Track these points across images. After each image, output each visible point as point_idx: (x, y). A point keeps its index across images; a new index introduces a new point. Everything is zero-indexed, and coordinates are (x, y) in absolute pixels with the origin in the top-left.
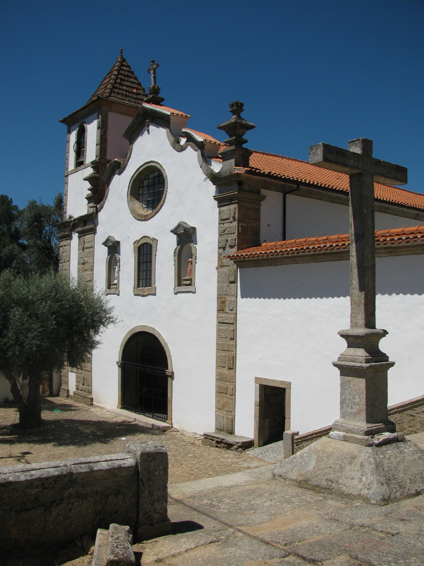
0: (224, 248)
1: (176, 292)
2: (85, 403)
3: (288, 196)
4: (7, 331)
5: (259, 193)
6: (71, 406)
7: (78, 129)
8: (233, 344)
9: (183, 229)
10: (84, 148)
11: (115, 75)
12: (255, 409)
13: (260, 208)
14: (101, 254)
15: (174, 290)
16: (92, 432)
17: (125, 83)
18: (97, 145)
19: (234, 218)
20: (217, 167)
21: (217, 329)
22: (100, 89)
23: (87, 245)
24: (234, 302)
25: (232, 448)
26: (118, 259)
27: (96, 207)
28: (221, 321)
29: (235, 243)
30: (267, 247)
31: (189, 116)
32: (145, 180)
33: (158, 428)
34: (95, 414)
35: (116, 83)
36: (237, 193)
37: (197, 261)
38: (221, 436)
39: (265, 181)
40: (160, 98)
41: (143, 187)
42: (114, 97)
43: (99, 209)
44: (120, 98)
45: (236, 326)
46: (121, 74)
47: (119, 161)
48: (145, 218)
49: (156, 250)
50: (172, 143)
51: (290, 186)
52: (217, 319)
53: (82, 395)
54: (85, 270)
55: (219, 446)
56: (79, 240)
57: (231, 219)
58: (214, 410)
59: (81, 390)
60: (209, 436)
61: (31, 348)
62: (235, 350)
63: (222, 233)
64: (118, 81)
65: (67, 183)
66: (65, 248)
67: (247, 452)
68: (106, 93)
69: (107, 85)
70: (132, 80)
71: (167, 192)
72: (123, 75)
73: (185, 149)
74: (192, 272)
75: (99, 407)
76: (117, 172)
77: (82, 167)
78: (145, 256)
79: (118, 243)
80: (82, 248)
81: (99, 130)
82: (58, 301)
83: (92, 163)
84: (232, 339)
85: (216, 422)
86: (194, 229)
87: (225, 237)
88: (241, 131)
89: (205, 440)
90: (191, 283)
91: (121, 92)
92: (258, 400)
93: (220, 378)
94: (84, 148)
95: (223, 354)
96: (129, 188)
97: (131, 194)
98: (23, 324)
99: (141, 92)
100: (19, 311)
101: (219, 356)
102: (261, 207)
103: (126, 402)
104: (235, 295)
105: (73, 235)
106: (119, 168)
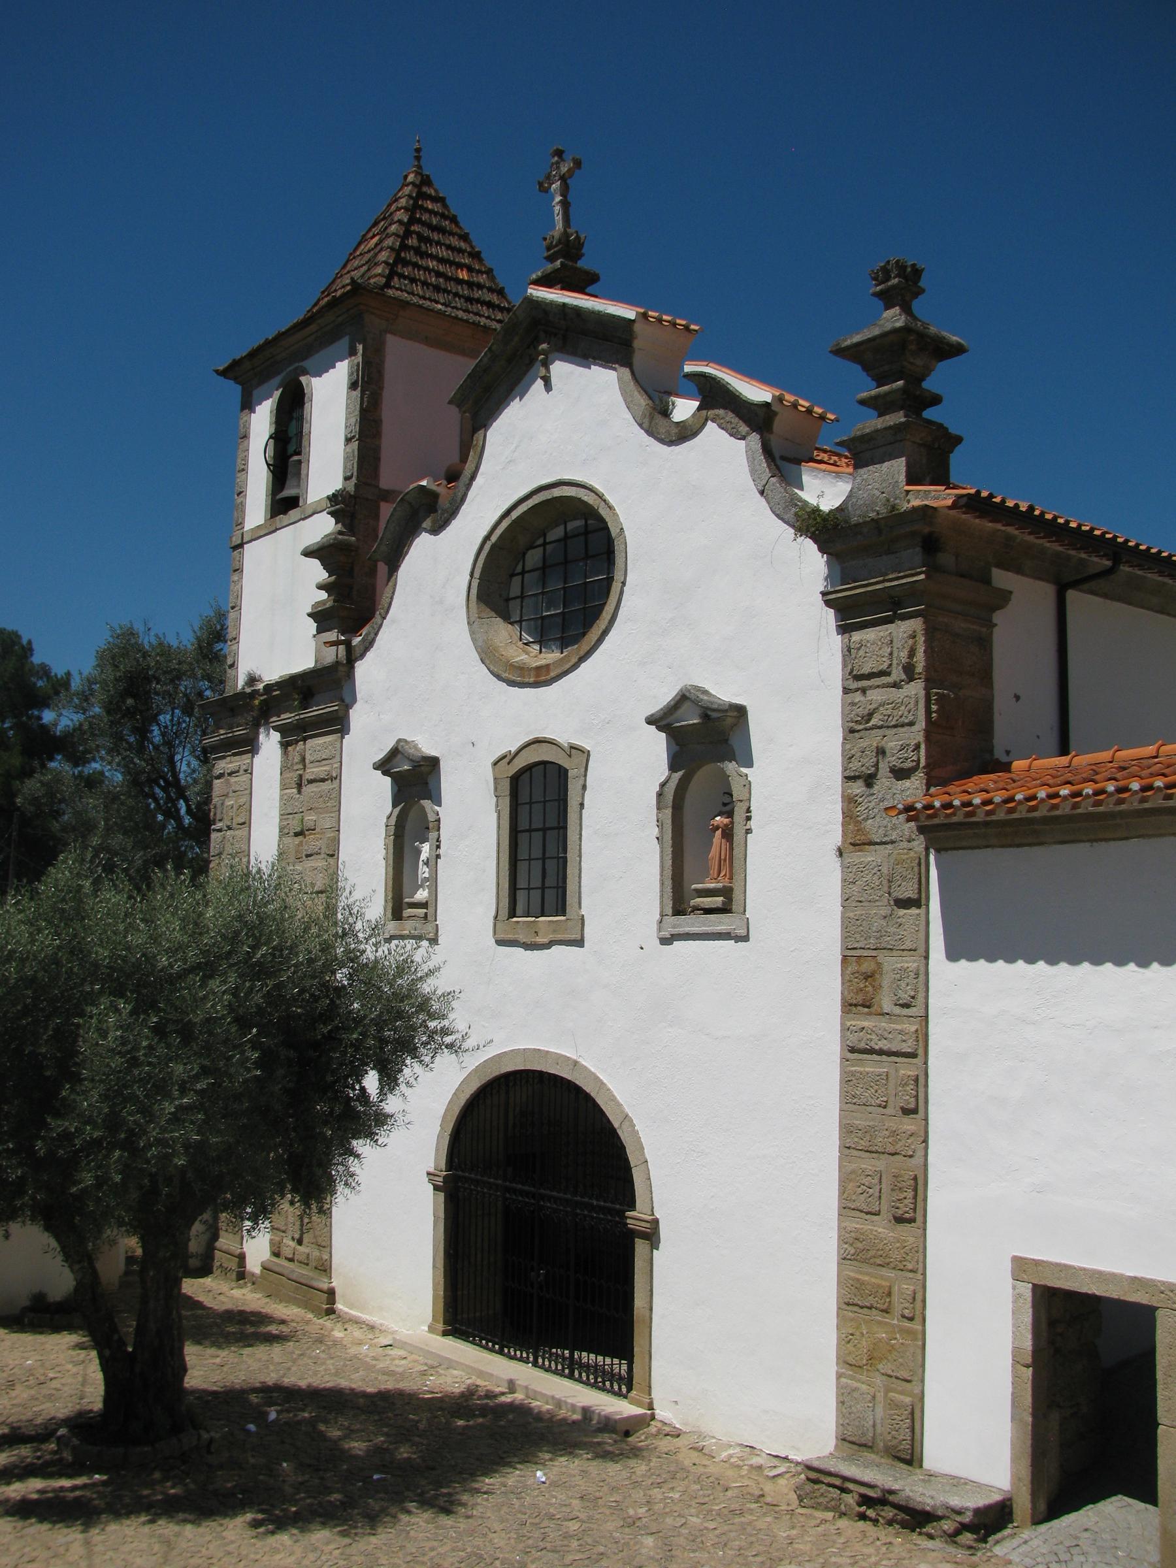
0: (869, 780)
1: (666, 934)
2: (306, 1305)
3: (1071, 595)
4: (72, 1090)
5: (987, 580)
6: (261, 1318)
7: (277, 394)
8: (912, 1128)
9: (698, 711)
10: (299, 453)
11: (400, 222)
12: (1016, 1376)
13: (991, 633)
14: (366, 802)
15: (660, 930)
16: (378, 1450)
17: (433, 250)
18: (348, 440)
19: (909, 670)
20: (824, 490)
21: (843, 1072)
22: (348, 268)
23: (313, 771)
24: (917, 974)
25: (928, 1529)
26: (431, 817)
27: (348, 644)
28: (862, 1045)
29: (919, 760)
30: (1034, 774)
31: (697, 328)
32: (532, 547)
33: (608, 1425)
34: (355, 1356)
35: (404, 247)
36: (922, 577)
37: (753, 824)
38: (877, 1474)
39: (1010, 537)
40: (587, 273)
41: (523, 573)
42: (402, 291)
43: (358, 652)
44: (421, 293)
45: (926, 1063)
46: (419, 221)
47: (433, 487)
48: (538, 676)
49: (584, 787)
50: (644, 416)
51: (1081, 559)
52: (843, 1037)
53: (294, 1277)
54: (307, 856)
55: (871, 1513)
56: (285, 752)
57: (897, 674)
58: (831, 1367)
59: (291, 1260)
60: (830, 1474)
61: (167, 1158)
62: (920, 1153)
63: (856, 726)
64: (412, 241)
65: (239, 570)
66: (233, 780)
67: (998, 1550)
68: (376, 276)
69: (376, 255)
70: (454, 241)
71: (624, 583)
72: (426, 223)
73: (695, 434)
74: (732, 861)
75: (357, 1322)
76: (427, 524)
77: (294, 514)
78: (537, 808)
79: (433, 763)
80: (297, 781)
81: (357, 393)
82: (260, 971)
83: (333, 498)
84: (906, 1112)
85: (840, 1414)
86: (740, 712)
87: (872, 740)
88: (919, 362)
89: (809, 1487)
90: (727, 902)
91: (421, 275)
92: (1028, 1343)
93: (856, 1253)
94: (299, 453)
95: (869, 1164)
96: (472, 575)
97: (480, 597)
98: (134, 1062)
99: (482, 279)
100: (117, 1010)
101: (853, 1172)
102: (996, 630)
103: (461, 1315)
104: (921, 951)
105: (262, 737)
106: (432, 511)
